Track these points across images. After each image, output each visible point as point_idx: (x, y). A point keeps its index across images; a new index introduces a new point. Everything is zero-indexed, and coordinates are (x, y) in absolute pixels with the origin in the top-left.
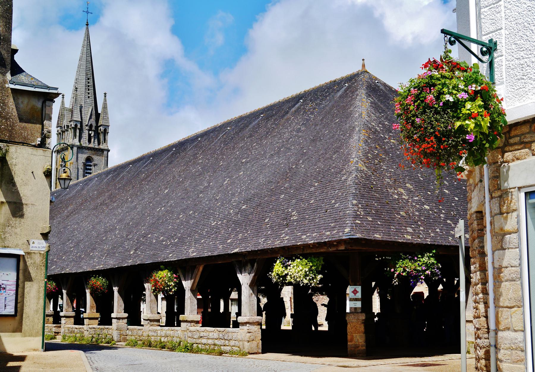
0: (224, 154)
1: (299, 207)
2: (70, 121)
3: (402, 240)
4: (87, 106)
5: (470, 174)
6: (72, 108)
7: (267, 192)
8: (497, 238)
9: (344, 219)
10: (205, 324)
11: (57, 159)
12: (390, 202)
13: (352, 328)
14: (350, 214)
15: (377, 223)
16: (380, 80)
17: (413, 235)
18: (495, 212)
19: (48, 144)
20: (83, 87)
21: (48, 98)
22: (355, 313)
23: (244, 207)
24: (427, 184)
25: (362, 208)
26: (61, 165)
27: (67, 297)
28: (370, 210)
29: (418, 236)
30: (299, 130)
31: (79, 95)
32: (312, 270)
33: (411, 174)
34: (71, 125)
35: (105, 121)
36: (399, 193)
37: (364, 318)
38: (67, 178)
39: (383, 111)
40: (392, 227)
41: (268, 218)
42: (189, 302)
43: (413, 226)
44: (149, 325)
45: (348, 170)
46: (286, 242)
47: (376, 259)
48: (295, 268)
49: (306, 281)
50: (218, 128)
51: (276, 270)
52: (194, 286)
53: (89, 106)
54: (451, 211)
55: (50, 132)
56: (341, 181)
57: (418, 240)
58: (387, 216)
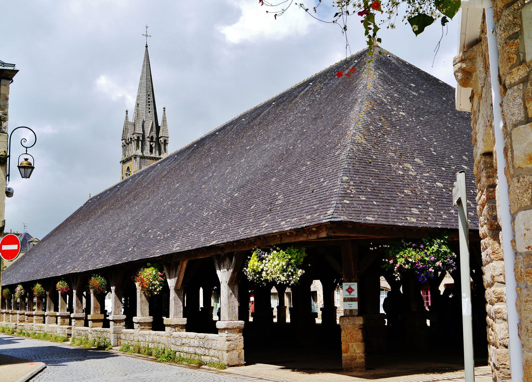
0: (233, 145)
1: (286, 190)
2: (133, 134)
3: (403, 223)
4: (148, 120)
5: (468, 78)
6: (135, 122)
7: (261, 177)
8: (521, 180)
9: (329, 200)
10: (188, 328)
11: (123, 168)
12: (393, 178)
13: (347, 335)
14: (337, 192)
15: (372, 203)
16: (392, 54)
17: (419, 217)
18: (514, 118)
19: (4, 128)
20: (144, 103)
21: (3, 75)
22: (351, 316)
23: (236, 195)
24: (441, 159)
25: (354, 186)
26: (127, 174)
27: (76, 298)
28: (365, 188)
29: (426, 218)
30: (304, 111)
31: (141, 110)
32: (291, 264)
33: (422, 147)
34: (134, 137)
35: (165, 133)
36: (405, 168)
37: (361, 323)
38: (27, 165)
39: (393, 84)
40: (391, 208)
41: (255, 204)
42: (173, 303)
43: (420, 206)
44: (139, 329)
45: (344, 144)
46: (264, 229)
47: (370, 249)
48: (271, 261)
49: (283, 279)
50: (234, 121)
51: (251, 265)
52: (179, 285)
53: (150, 120)
54: (470, 189)
55: (6, 115)
56: (334, 157)
57: (425, 223)
58: (387, 195)
